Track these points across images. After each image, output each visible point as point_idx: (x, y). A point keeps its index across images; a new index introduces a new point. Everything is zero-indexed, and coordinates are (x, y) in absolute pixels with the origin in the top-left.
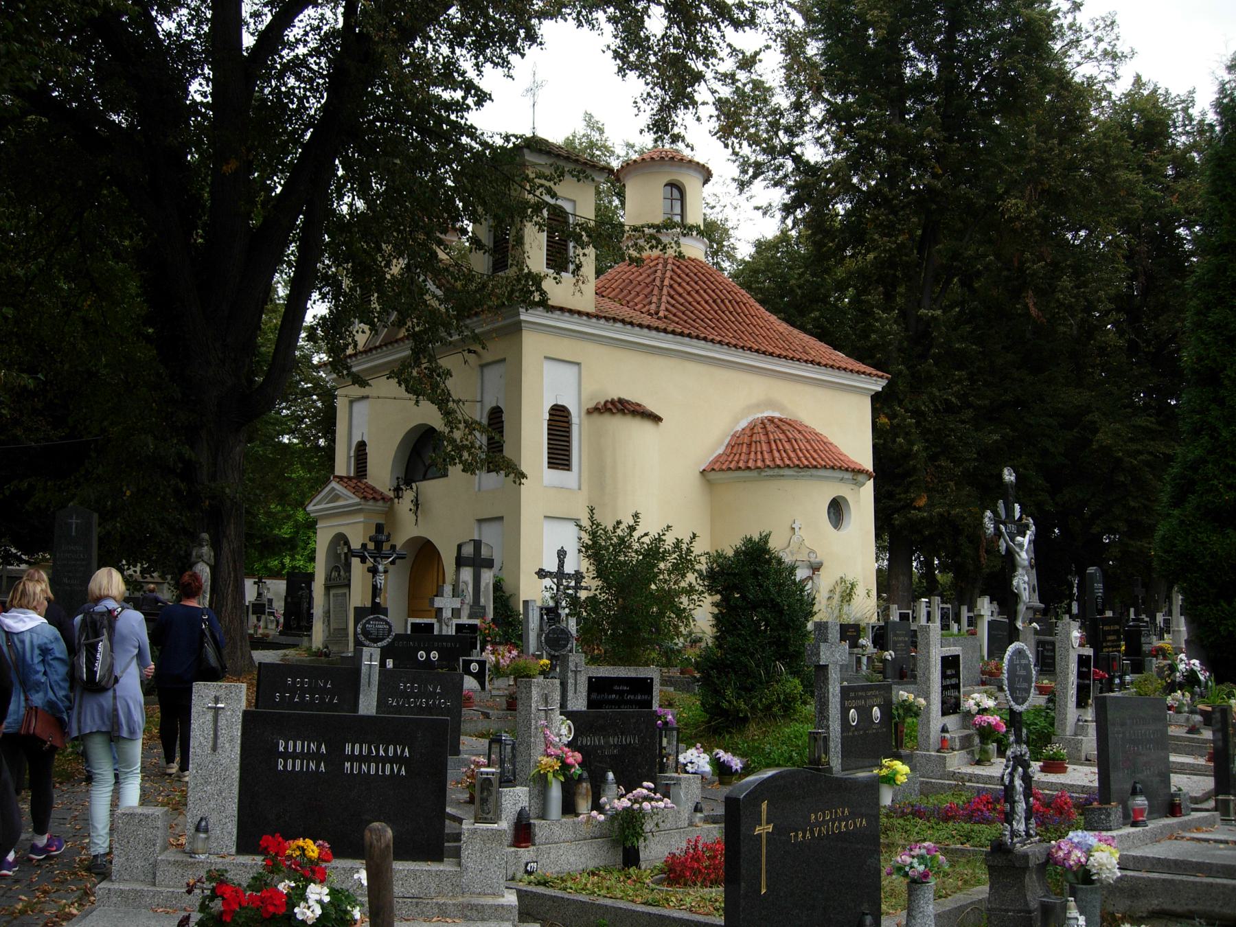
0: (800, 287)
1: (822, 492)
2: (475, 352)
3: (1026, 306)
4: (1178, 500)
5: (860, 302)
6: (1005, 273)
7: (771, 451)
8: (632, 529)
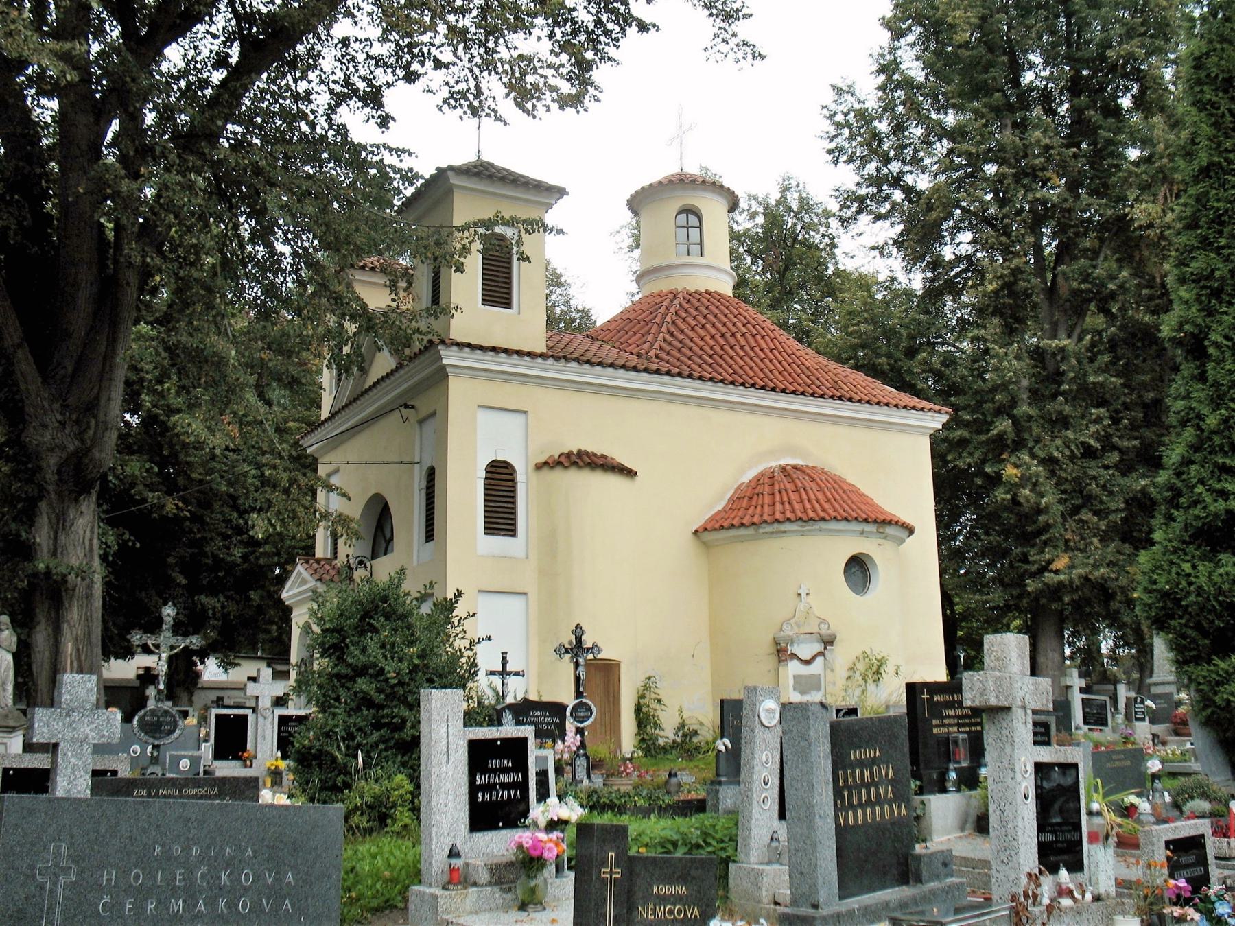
2: (413, 407)
7: (802, 501)
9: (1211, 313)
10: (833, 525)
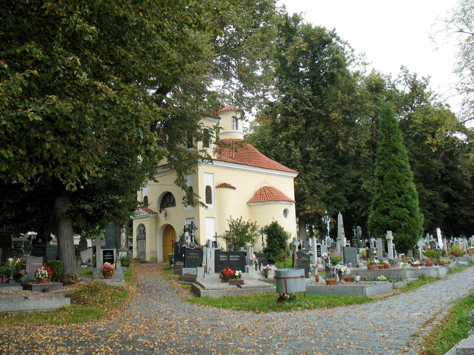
0: (269, 142)
1: (281, 207)
3: (339, 146)
4: (374, 209)
5: (287, 145)
6: (332, 136)
8: (240, 220)
9: (384, 172)
10: (281, 202)
